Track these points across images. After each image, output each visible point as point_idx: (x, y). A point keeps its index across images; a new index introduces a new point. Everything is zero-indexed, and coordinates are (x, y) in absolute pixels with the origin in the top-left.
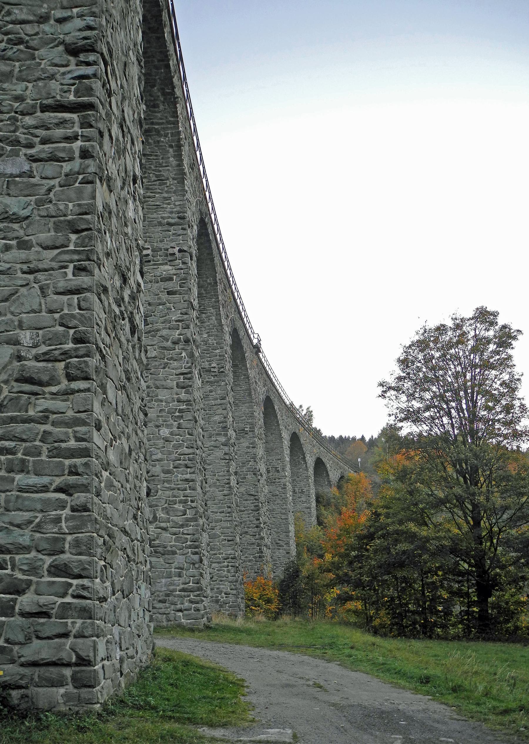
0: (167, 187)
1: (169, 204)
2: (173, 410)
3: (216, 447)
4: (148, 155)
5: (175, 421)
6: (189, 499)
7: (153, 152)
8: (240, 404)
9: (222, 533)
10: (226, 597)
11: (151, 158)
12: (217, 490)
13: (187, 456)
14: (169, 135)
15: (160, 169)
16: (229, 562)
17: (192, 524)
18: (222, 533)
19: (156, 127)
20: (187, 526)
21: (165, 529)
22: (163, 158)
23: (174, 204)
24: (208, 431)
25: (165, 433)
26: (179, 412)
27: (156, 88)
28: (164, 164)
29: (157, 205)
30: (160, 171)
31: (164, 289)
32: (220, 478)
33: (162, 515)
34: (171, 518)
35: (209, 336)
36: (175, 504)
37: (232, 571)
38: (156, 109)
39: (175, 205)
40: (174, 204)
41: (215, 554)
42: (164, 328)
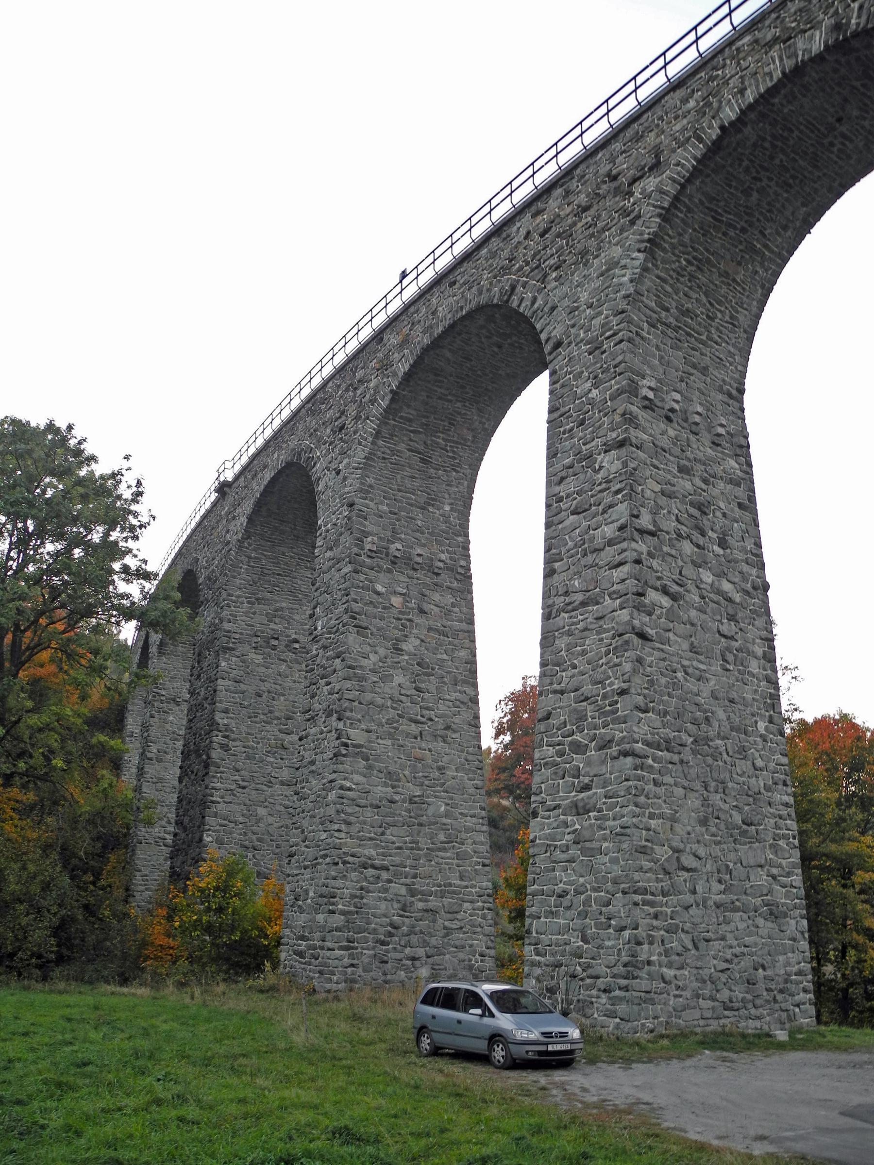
3: (462, 703)
4: (737, 282)
5: (767, 711)
7: (743, 282)
8: (304, 601)
9: (475, 852)
10: (482, 961)
12: (466, 777)
14: (770, 272)
15: (739, 309)
16: (484, 902)
18: (475, 852)
19: (767, 253)
21: (774, 877)
22: (748, 297)
23: (736, 367)
24: (451, 672)
27: (805, 209)
28: (745, 306)
29: (721, 359)
30: (737, 312)
32: (470, 757)
33: (771, 856)
35: (452, 509)
37: (489, 917)
38: (783, 232)
40: (736, 367)
41: (467, 887)
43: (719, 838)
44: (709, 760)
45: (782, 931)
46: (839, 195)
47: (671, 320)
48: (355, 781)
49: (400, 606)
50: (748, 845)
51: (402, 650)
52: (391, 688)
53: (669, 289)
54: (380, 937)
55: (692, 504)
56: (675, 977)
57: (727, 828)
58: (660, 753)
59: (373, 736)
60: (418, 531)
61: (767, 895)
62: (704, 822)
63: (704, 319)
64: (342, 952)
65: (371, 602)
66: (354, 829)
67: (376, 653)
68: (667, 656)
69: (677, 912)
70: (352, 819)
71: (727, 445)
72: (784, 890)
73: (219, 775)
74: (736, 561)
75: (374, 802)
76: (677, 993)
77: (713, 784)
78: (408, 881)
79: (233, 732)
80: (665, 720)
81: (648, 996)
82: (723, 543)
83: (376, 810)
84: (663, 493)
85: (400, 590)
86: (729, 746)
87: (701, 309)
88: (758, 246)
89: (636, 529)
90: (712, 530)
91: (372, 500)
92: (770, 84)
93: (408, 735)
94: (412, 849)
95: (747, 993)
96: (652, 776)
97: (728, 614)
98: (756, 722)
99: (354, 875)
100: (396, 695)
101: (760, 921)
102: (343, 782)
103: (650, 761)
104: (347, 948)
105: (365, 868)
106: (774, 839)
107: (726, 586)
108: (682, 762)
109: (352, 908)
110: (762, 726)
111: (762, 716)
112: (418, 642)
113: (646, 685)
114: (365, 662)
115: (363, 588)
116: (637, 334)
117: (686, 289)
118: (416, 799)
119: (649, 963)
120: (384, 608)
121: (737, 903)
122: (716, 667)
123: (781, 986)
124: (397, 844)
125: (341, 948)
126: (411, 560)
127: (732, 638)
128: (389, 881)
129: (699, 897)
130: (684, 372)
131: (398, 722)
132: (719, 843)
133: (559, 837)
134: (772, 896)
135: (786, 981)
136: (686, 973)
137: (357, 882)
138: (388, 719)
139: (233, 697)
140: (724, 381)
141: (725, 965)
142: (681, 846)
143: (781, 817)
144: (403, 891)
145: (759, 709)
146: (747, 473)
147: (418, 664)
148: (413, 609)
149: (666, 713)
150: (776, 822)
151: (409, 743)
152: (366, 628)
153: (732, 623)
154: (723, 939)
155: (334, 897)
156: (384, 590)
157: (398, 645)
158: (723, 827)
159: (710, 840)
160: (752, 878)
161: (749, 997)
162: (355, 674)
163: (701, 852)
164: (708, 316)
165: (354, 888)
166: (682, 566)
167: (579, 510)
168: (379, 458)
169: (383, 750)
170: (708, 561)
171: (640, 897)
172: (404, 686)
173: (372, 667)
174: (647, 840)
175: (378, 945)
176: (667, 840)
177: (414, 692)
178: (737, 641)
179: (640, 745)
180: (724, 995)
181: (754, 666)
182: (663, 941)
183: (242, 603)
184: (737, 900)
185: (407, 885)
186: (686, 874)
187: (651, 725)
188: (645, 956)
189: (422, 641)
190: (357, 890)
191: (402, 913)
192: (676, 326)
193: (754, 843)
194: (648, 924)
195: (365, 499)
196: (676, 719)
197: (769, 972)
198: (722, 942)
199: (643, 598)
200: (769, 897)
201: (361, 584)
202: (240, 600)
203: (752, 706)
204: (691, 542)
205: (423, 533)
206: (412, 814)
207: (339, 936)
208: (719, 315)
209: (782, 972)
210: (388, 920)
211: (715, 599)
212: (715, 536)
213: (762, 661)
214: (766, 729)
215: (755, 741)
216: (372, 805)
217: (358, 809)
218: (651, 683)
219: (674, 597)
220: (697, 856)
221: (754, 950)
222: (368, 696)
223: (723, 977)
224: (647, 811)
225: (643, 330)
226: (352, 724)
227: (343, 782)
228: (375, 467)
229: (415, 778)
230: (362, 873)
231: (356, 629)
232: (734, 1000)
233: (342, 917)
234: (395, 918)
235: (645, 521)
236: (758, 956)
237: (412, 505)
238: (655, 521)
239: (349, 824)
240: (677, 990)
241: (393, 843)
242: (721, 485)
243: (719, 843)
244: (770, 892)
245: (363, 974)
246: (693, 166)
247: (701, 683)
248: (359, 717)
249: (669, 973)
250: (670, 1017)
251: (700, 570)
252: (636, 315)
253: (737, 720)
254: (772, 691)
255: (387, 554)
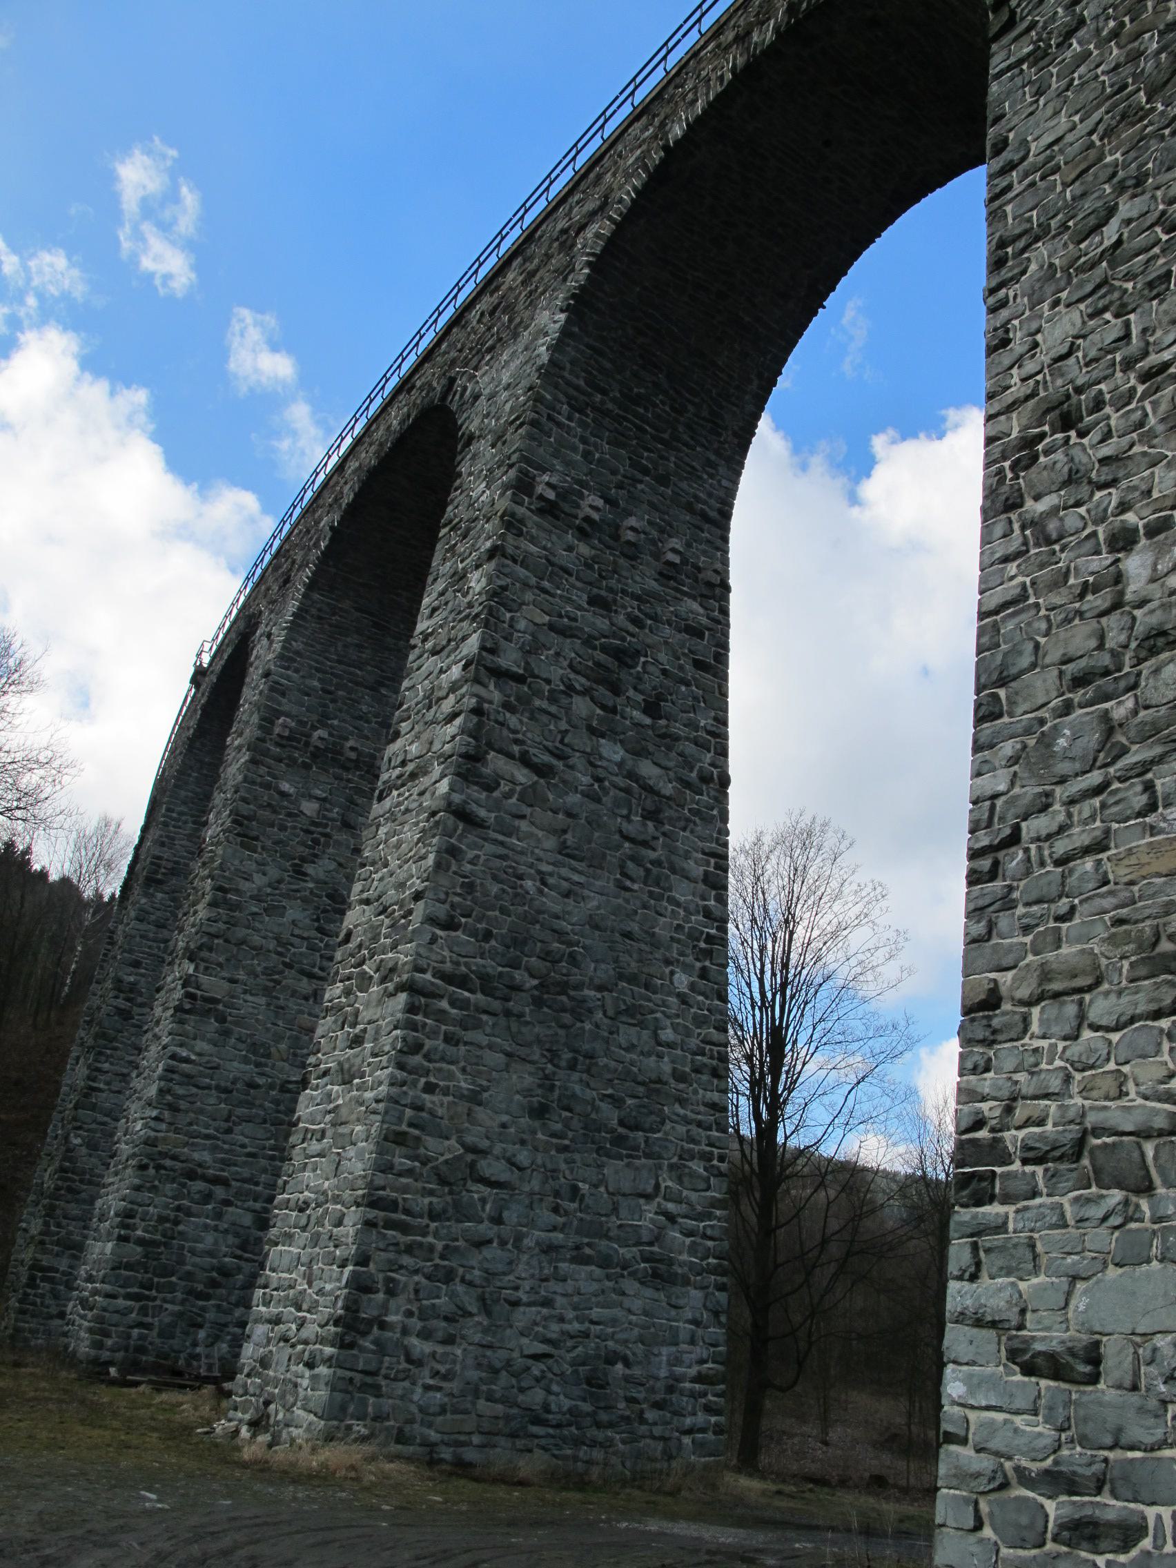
0: (720, 442)
1: (711, 476)
2: (697, 935)
5: (697, 959)
6: (716, 1151)
11: (721, 375)
13: (715, 1048)
14: (769, 357)
15: (724, 403)
17: (718, 1213)
20: (709, 1216)
21: (671, 1218)
25: (682, 983)
26: (706, 942)
29: (693, 467)
31: (690, 651)
33: (670, 1183)
34: (685, 1193)
36: (692, 1158)
39: (720, 485)
40: (719, 481)
42: (687, 739)
43: (566, 1142)
44: (567, 1018)
45: (675, 1307)
46: (856, 255)
47: (610, 406)
48: (197, 1049)
49: (314, 815)
50: (626, 1160)
51: (305, 874)
52: (280, 925)
53: (608, 365)
54: (196, 1285)
55: (605, 649)
56: (434, 1354)
57: (585, 1128)
58: (466, 994)
59: (239, 988)
60: (360, 718)
61: (651, 1244)
62: (540, 1112)
63: (665, 411)
64: (129, 1303)
65: (269, 805)
66: (182, 1120)
67: (264, 874)
68: (511, 853)
69: (456, 1249)
70: (183, 1105)
71: (687, 581)
72: (688, 1241)
73: (108, 1052)
74: (677, 739)
75: (223, 1084)
76: (431, 1382)
77: (567, 1055)
78: (258, 1206)
79: (141, 994)
80: (487, 946)
81: (369, 1380)
82: (652, 709)
83: (223, 1096)
84: (551, 627)
85: (318, 792)
86: (609, 1002)
87: (661, 397)
88: (747, 319)
89: (486, 668)
90: (635, 689)
91: (297, 671)
92: (719, 89)
93: (294, 994)
94: (272, 1158)
95: (584, 1400)
96: (444, 1027)
97: (643, 809)
98: (672, 973)
99: (169, 1188)
100: (286, 936)
101: (630, 1286)
102: (178, 1050)
103: (444, 1004)
104: (136, 1297)
105: (191, 1180)
106: (681, 1158)
107: (647, 769)
108: (508, 1013)
109: (158, 1237)
110: (682, 981)
111: (687, 968)
112: (333, 866)
113: (459, 890)
114: (245, 886)
115: (261, 785)
116: (550, 418)
117: (635, 367)
118: (291, 1086)
119: (383, 1326)
120: (290, 815)
121: (587, 1251)
122: (605, 881)
123: (658, 1397)
124: (249, 1150)
125: (128, 1297)
126: (342, 754)
127: (645, 844)
128: (227, 1203)
129: (505, 1230)
130: (625, 476)
131: (281, 973)
132: (566, 1149)
133: (319, 1118)
134: (660, 1247)
135: (670, 1389)
136: (459, 1352)
137: (174, 1198)
138: (266, 968)
139: (150, 947)
140: (696, 497)
141: (541, 1348)
142: (484, 1144)
143: (700, 1124)
144: (247, 1220)
145: (682, 954)
146: (719, 622)
147: (328, 896)
148: (333, 820)
149: (488, 935)
150: (688, 1131)
151: (293, 1005)
152: (256, 839)
153: (650, 824)
154: (547, 1303)
155: (132, 1217)
156: (292, 790)
157: (301, 866)
158: (575, 1123)
159: (547, 1142)
160: (623, 1212)
161: (586, 1407)
162: (225, 899)
163: (523, 1157)
164: (672, 408)
165: (166, 1206)
166: (567, 731)
167: (438, 648)
168: (312, 616)
169: (251, 1010)
170: (619, 729)
171: (382, 1214)
172: (300, 925)
173: (255, 892)
174: (410, 1125)
175: (191, 1298)
176: (459, 1131)
177: (313, 933)
178: (654, 849)
179: (428, 976)
180: (536, 1397)
181: (683, 892)
182: (417, 1291)
183: (186, 822)
184: (589, 1245)
185: (254, 1211)
186: (486, 1190)
187: (455, 949)
188: (375, 1313)
189: (340, 865)
190: (172, 1210)
191: (239, 1252)
192: (618, 415)
193: (639, 1158)
194: (390, 1261)
195: (287, 668)
196: (508, 947)
197: (637, 1371)
198: (545, 1311)
199: (479, 765)
200: (656, 1249)
201: (259, 780)
202: (184, 818)
203: (669, 948)
204: (592, 699)
205: (368, 722)
206: (282, 1108)
207: (128, 1278)
208: (690, 408)
209: (663, 1373)
210: (215, 1261)
211: (622, 785)
212: (640, 698)
213: (701, 886)
214: (692, 987)
215: (664, 1001)
216: (218, 1088)
217: (194, 1090)
218: (469, 888)
219: (542, 771)
220: (513, 1164)
221: (610, 1330)
222: (241, 932)
223: (537, 1369)
224: (423, 1080)
225: (559, 413)
226: (207, 968)
227: (178, 1050)
228: (306, 628)
229: (295, 1055)
230: (184, 1185)
231: (239, 839)
232: (553, 1407)
233: (139, 1249)
234: (227, 1259)
235: (509, 659)
236: (617, 1341)
237: (357, 684)
238: (527, 663)
239: (176, 1110)
240: (432, 1377)
241: (243, 1146)
242: (667, 631)
243: (566, 1149)
244: (657, 1239)
245: (157, 1341)
246: (632, 199)
247: (571, 901)
248: (221, 959)
249: (419, 1346)
250: (411, 1421)
251: (603, 741)
252: (549, 393)
253: (633, 964)
254: (713, 931)
255: (307, 744)
